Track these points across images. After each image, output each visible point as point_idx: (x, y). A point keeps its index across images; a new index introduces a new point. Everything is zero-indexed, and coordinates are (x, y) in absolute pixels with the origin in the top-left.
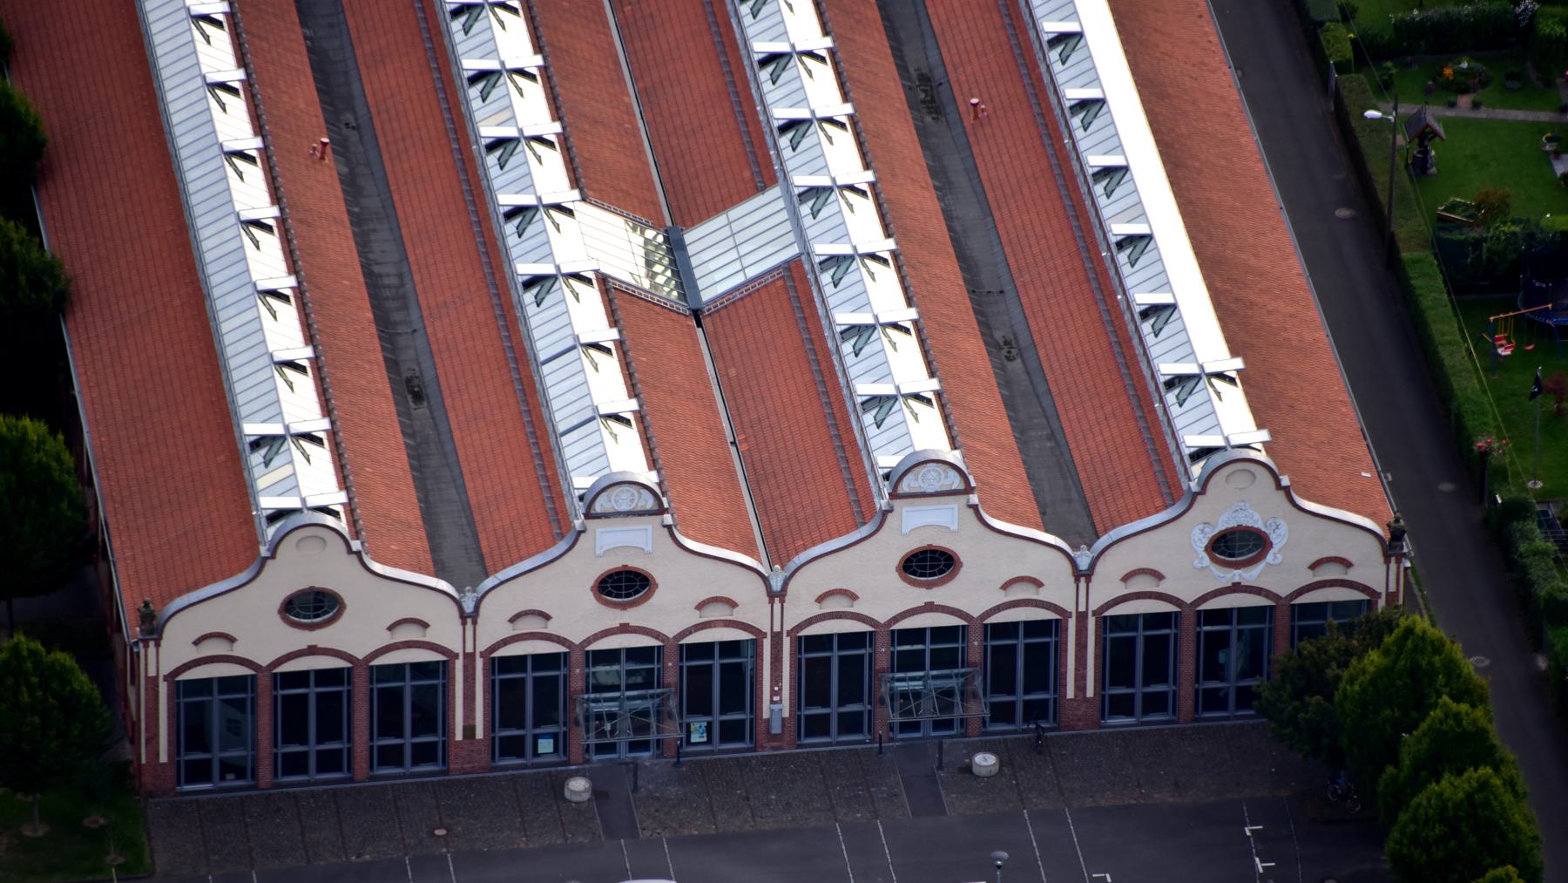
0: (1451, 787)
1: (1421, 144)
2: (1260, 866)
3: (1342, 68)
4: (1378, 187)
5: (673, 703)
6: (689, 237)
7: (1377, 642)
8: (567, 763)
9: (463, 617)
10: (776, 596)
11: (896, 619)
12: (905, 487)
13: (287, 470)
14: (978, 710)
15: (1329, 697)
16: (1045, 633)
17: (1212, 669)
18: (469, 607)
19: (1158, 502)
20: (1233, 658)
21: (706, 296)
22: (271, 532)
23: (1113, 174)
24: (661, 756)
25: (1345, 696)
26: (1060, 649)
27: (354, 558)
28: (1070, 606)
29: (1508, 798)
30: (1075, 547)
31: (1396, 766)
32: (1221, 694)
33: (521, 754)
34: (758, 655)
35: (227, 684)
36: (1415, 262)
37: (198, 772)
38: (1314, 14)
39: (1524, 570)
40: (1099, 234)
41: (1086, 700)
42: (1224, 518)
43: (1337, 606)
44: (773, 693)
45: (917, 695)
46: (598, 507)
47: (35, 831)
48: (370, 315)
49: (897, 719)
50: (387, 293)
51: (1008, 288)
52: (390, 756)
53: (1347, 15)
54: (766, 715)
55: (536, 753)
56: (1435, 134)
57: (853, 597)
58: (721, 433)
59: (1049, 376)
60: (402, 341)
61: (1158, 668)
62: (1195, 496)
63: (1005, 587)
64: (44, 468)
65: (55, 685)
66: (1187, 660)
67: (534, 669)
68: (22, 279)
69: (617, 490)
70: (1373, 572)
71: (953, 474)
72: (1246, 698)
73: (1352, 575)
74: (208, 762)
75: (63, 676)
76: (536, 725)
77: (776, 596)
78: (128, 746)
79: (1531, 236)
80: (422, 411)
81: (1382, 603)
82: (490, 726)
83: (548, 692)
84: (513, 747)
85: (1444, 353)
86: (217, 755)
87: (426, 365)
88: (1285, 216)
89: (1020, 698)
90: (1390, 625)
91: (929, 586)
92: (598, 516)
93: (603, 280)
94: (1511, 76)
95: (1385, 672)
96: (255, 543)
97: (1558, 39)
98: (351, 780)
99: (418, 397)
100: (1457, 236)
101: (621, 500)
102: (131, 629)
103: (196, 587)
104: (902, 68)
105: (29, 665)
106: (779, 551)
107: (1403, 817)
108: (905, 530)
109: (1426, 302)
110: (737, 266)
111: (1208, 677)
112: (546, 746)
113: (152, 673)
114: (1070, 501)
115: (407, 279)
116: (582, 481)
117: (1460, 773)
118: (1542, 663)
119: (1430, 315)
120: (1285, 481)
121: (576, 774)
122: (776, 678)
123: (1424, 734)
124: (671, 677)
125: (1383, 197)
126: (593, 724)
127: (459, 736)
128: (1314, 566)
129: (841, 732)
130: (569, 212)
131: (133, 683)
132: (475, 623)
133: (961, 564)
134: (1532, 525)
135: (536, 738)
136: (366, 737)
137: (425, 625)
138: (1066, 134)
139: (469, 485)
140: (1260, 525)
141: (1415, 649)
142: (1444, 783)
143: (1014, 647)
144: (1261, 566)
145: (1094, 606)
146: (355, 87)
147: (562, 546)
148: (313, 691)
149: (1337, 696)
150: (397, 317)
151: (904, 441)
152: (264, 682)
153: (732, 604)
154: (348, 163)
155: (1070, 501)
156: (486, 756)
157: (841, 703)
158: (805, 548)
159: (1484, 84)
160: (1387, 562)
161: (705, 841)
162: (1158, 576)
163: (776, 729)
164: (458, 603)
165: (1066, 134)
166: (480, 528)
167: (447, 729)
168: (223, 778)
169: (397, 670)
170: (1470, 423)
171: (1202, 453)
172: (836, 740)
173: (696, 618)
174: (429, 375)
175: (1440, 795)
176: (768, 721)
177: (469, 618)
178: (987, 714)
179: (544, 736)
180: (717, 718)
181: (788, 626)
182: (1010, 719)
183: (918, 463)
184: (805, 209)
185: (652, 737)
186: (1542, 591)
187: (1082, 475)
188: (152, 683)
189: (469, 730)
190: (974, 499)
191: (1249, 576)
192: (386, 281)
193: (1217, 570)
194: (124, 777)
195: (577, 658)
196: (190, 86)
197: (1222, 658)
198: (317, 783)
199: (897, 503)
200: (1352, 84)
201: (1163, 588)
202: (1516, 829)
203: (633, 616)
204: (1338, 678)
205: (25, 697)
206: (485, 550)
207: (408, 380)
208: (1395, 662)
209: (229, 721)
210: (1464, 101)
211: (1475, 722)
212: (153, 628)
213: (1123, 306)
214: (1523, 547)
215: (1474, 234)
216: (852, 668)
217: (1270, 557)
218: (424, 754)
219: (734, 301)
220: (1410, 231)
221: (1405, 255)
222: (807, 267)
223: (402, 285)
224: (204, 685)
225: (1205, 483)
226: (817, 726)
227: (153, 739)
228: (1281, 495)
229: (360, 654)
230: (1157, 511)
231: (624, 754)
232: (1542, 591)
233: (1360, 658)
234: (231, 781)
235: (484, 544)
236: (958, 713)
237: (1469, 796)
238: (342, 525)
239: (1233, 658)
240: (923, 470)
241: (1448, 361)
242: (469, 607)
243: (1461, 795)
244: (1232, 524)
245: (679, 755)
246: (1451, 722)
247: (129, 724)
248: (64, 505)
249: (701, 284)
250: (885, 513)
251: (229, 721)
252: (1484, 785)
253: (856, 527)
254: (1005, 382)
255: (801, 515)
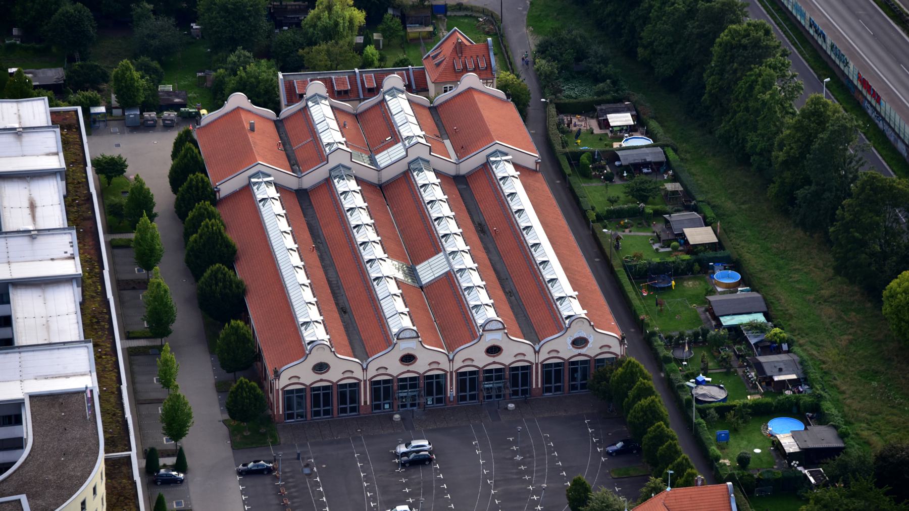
0: (644, 402)
1: (617, 241)
2: (590, 431)
3: (593, 222)
4: (607, 252)
5: (422, 392)
6: (417, 268)
7: (621, 365)
8: (393, 411)
9: (363, 369)
10: (451, 361)
11: (485, 366)
12: (486, 328)
13: (312, 330)
14: (508, 392)
15: (608, 382)
16: (526, 369)
17: (573, 379)
18: (365, 366)
19: (557, 331)
20: (579, 375)
21: (424, 283)
22: (309, 347)
23: (536, 245)
24: (419, 408)
25: (612, 381)
26: (531, 374)
27: (333, 353)
28: (533, 361)
29: (659, 405)
30: (535, 345)
31: (628, 398)
32: (576, 386)
33: (380, 409)
34: (446, 378)
35: (298, 391)
36: (619, 271)
37: (290, 416)
38: (585, 208)
39: (656, 350)
40: (533, 262)
41: (538, 388)
42: (576, 334)
43: (608, 359)
44: (451, 389)
45: (491, 388)
46: (400, 336)
47: (247, 433)
48: (330, 291)
49: (485, 395)
50: (334, 286)
51: (509, 277)
52: (343, 410)
53: (593, 209)
54: (449, 395)
55: (384, 409)
56: (621, 238)
57: (473, 360)
58: (431, 318)
59: (523, 300)
60: (339, 298)
61: (558, 379)
62: (568, 328)
63: (515, 356)
64: (244, 334)
65: (252, 391)
66: (566, 376)
67: (383, 384)
68: (234, 285)
69: (406, 331)
70: (617, 349)
71: (500, 324)
72: (583, 386)
73: (611, 350)
74: (293, 413)
75: (254, 388)
76: (384, 400)
77: (451, 361)
78: (270, 411)
79: (650, 263)
80: (347, 316)
81: (620, 357)
82: (371, 401)
83: (387, 391)
84: (378, 407)
85: (629, 294)
86: (296, 411)
87: (346, 304)
88: (583, 257)
89: (520, 388)
90: (623, 362)
91: (494, 356)
92: (401, 339)
93: (395, 278)
94: (639, 224)
95: (623, 374)
96: (304, 351)
97: (651, 214)
98: (333, 418)
99: (345, 312)
100: (629, 264)
101: (407, 334)
102: (270, 375)
103: (288, 363)
104: (473, 222)
105: (245, 386)
106: (451, 347)
107: (631, 411)
108: (487, 340)
109: (623, 281)
110: (432, 274)
111: (572, 381)
112: (387, 406)
113: (277, 388)
114: (531, 333)
115: (339, 282)
116: (395, 330)
117: (646, 399)
118: (662, 375)
119: (624, 285)
120: (592, 324)
121: (396, 413)
122: (451, 385)
123: (635, 389)
124: (422, 385)
125: (608, 254)
126: (400, 400)
127: (363, 404)
128: (601, 348)
129: (470, 400)
130: (385, 261)
131: (271, 392)
132: (366, 371)
133: (503, 350)
134: (657, 338)
135: (384, 404)
136: (337, 405)
137: (352, 372)
138: (522, 236)
139: (362, 335)
140: (586, 336)
141: (632, 366)
142: (642, 401)
143: (518, 374)
144: (586, 348)
145: (540, 361)
146: (320, 232)
147: (390, 348)
148: (321, 392)
149: (610, 381)
150: (338, 291)
151: (485, 316)
152: (308, 390)
153: (439, 363)
154: (320, 252)
155: (531, 333)
156: (370, 409)
157: (470, 391)
158: (458, 347)
159: (632, 226)
160: (621, 346)
161: (433, 430)
162: (558, 352)
163: (452, 399)
164: (362, 366)
165: (522, 236)
166: (366, 345)
167: (359, 402)
168: (297, 418)
169: (345, 385)
170: (638, 312)
171: (569, 317)
172: (468, 402)
173: (428, 368)
174: (347, 306)
175: (641, 405)
176: (449, 397)
177: (365, 370)
178: (511, 392)
179: (386, 403)
180: (435, 397)
181: (454, 370)
182: (517, 395)
183: (490, 321)
184: (451, 257)
185: (417, 402)
186: (662, 355)
187: (534, 326)
188: (278, 391)
189: (365, 402)
190: (506, 331)
191: (583, 351)
192: (333, 282)
193: (574, 350)
194: (269, 420)
195: (395, 380)
196: (277, 232)
197: (576, 376)
198: (323, 419)
199: (484, 333)
200: (597, 226)
201: (559, 355)
202: (662, 412)
203: (411, 368)
204: (610, 377)
205: (245, 395)
206: (368, 351)
207: (342, 308)
208: (626, 371)
209: (298, 402)
210: (627, 230)
211: (649, 385)
212: (277, 375)
213: (542, 280)
214: (655, 344)
215: (635, 263)
216: (472, 381)
217: (589, 345)
218: (353, 410)
219: (432, 284)
220: (616, 263)
221: (616, 269)
222: (452, 273)
223: (338, 283)
224: (292, 391)
225: (570, 325)
226: (463, 398)
227: (278, 407)
228: (591, 327)
229: (335, 381)
230: (556, 333)
231: (409, 408)
232: (662, 355)
233: (616, 370)
234: (299, 419)
235: (367, 350)
236: (502, 393)
237: (649, 404)
238: (328, 344)
239: (579, 375)
240: (491, 323)
241: (630, 296)
242: (365, 366)
243: (647, 404)
244: (578, 336)
245: (425, 408)
246: (643, 385)
247: (270, 404)
248: (250, 345)
249: (422, 280)
250: (481, 336)
251: (298, 402)
252: (653, 401)
253: (472, 340)
254: (510, 302)
255: (456, 339)
